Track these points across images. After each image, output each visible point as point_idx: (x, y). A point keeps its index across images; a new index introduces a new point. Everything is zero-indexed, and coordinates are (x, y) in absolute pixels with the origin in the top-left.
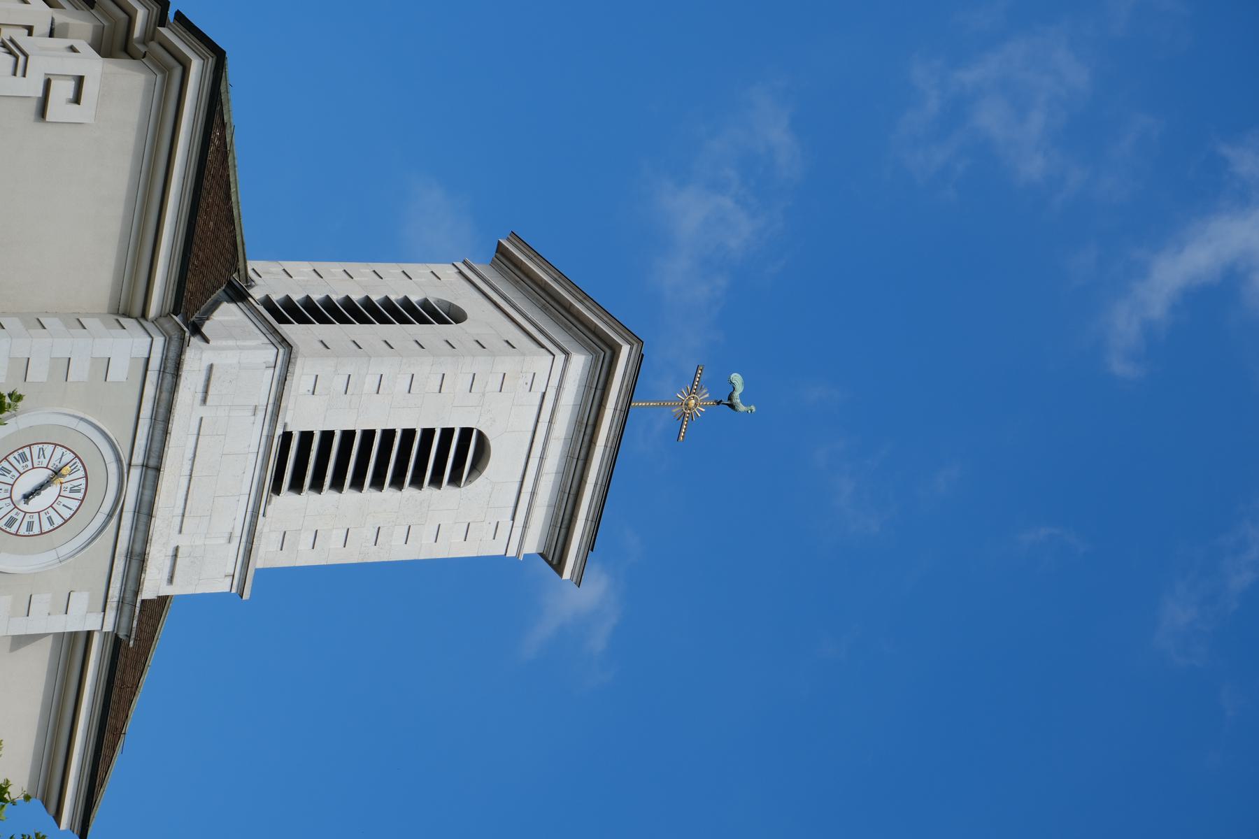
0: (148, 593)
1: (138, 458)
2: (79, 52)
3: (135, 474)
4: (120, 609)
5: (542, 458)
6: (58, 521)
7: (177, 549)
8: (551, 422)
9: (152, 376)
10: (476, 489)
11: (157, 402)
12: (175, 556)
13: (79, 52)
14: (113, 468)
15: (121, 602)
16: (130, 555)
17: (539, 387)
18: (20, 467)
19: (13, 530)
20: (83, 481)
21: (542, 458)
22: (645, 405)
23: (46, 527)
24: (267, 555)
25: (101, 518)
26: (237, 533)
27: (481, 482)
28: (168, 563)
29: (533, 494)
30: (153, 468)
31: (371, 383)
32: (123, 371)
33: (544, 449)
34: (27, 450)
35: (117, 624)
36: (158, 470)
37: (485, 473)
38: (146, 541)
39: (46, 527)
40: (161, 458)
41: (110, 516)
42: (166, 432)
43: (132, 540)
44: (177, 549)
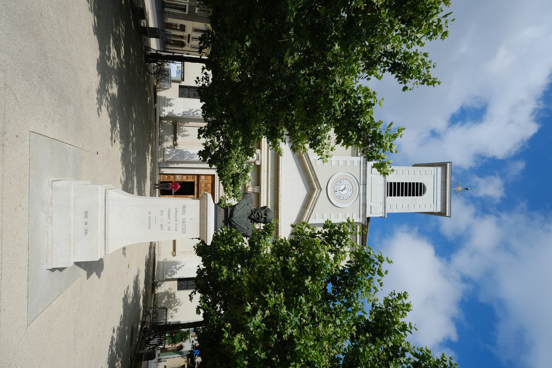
0: (367, 216)
1: (362, 183)
2: (87, 279)
3: (361, 186)
4: (363, 217)
5: (437, 189)
6: (348, 197)
7: (371, 206)
8: (437, 181)
9: (362, 165)
10: (424, 196)
11: (363, 170)
12: (371, 208)
13: (87, 279)
14: (357, 185)
15: (363, 215)
16: (363, 204)
17: (433, 174)
18: (340, 184)
19: (340, 198)
20: (352, 188)
21: (437, 189)
22: (328, 37)
23: (346, 198)
24: (389, 210)
25: (356, 196)
26: (382, 203)
27: (424, 196)
28: (370, 209)
29: (436, 197)
30: (365, 184)
31: (401, 172)
32: (356, 164)
33: (437, 187)
34: (338, 197)
35: (363, 221)
36: (366, 184)
37: (426, 193)
38: (366, 200)
39: (346, 198)
40: (366, 182)
41: (358, 196)
42: (366, 176)
43: (363, 201)
44: (371, 206)
